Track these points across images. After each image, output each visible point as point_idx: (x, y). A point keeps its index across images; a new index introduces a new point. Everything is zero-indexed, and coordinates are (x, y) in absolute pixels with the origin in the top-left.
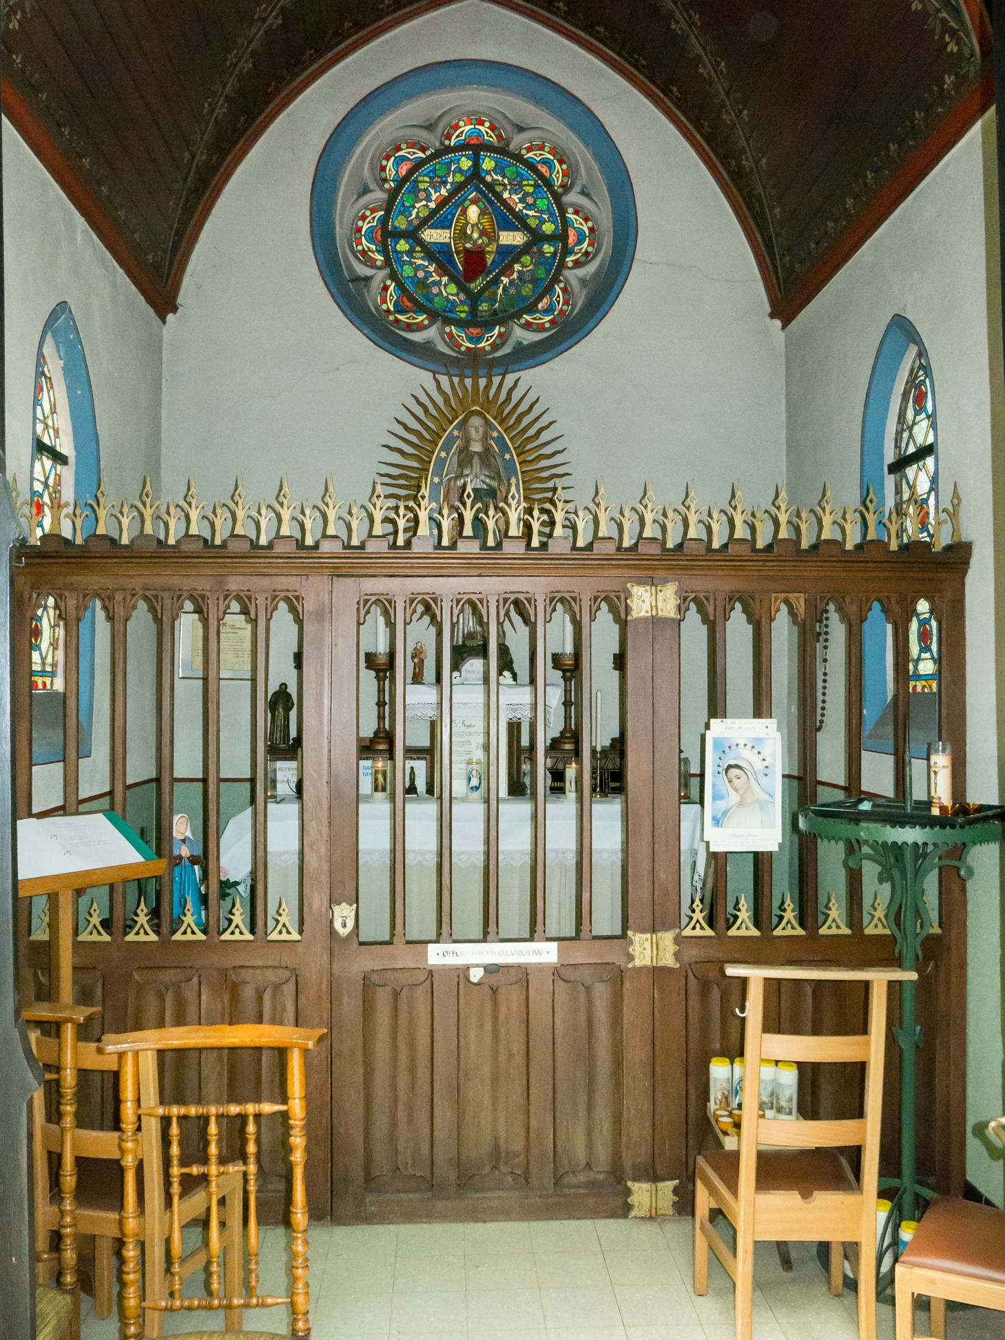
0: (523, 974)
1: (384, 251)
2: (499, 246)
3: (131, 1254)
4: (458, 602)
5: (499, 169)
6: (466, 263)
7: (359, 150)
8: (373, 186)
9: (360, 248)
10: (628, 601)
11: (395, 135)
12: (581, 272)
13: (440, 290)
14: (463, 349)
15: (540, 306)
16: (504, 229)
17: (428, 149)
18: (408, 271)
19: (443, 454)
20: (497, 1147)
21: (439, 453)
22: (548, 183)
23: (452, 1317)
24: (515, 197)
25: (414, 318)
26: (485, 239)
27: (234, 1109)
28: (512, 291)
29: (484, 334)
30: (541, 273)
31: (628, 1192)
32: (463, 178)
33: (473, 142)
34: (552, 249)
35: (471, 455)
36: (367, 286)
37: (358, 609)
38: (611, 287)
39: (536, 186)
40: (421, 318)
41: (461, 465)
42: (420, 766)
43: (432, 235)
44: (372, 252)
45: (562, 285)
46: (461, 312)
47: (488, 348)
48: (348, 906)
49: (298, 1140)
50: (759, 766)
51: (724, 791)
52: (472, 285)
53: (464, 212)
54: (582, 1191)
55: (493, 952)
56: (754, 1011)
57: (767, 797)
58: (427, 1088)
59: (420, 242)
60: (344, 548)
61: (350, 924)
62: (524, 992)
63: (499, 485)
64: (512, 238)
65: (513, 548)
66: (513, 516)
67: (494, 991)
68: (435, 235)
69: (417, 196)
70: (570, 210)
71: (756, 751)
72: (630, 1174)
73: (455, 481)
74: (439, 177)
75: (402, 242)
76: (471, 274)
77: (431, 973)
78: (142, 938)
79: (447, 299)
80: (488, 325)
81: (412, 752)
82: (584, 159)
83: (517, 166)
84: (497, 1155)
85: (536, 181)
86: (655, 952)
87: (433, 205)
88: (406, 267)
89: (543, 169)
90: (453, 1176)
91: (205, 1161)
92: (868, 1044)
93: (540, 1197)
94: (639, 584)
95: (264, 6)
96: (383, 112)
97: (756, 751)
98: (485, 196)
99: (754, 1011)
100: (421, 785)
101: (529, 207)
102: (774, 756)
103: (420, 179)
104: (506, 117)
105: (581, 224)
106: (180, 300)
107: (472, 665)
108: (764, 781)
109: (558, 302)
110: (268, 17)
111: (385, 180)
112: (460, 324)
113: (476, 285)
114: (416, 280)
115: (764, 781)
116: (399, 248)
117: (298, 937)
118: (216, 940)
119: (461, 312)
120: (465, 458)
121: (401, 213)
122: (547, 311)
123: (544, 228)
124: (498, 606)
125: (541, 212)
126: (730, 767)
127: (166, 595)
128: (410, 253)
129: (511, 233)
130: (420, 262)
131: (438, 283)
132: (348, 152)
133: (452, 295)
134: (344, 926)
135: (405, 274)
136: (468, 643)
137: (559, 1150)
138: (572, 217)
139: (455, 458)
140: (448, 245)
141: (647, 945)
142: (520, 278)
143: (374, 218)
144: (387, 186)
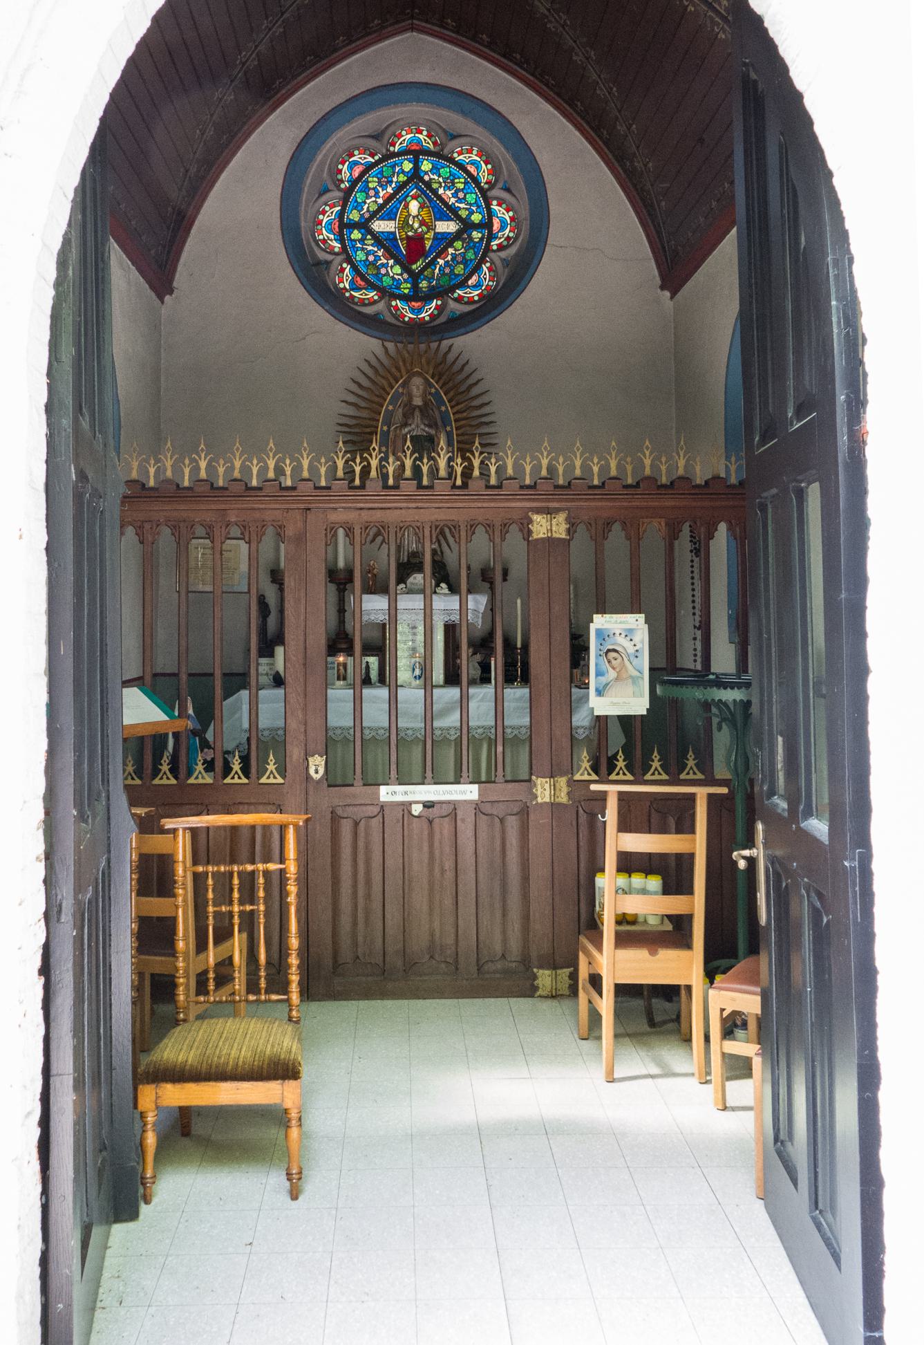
0: (453, 809)
1: (341, 240)
3: (181, 964)
4: (401, 528)
5: (435, 169)
6: (408, 248)
7: (319, 158)
8: (331, 186)
9: (321, 237)
10: (530, 526)
11: (350, 144)
12: (503, 254)
13: (387, 271)
14: (406, 319)
15: (470, 282)
17: (376, 155)
18: (361, 256)
19: (391, 408)
20: (432, 941)
21: (387, 406)
22: (475, 181)
23: (398, 1050)
24: (449, 193)
25: (366, 295)
27: (250, 868)
28: (447, 270)
29: (424, 306)
30: (470, 255)
31: (535, 977)
32: (406, 178)
33: (413, 148)
34: (480, 235)
36: (328, 268)
37: (326, 534)
38: (529, 265)
40: (372, 294)
42: (373, 661)
43: (380, 226)
44: (331, 240)
45: (488, 265)
46: (404, 288)
47: (427, 318)
48: (319, 758)
49: (292, 888)
50: (631, 650)
51: (605, 670)
52: (414, 267)
53: (406, 206)
54: (498, 976)
55: (429, 792)
56: (611, 815)
57: (638, 674)
59: (370, 232)
61: (322, 771)
62: (453, 823)
63: (436, 432)
65: (442, 487)
67: (431, 822)
68: (382, 226)
69: (367, 194)
70: (495, 202)
71: (628, 638)
72: (536, 963)
73: (401, 429)
74: (385, 177)
75: (356, 232)
78: (165, 781)
79: (393, 278)
80: (427, 298)
81: (368, 649)
83: (450, 167)
85: (466, 179)
86: (553, 792)
87: (380, 201)
88: (358, 253)
89: (472, 169)
90: (399, 963)
91: (231, 903)
92: (694, 841)
93: (467, 980)
94: (538, 513)
95: (244, 53)
96: (340, 126)
97: (628, 638)
98: (423, 192)
99: (611, 815)
100: (374, 674)
101: (460, 200)
102: (642, 642)
103: (370, 179)
104: (441, 127)
105: (503, 214)
106: (175, 284)
107: (415, 578)
108: (635, 661)
109: (485, 279)
110: (246, 61)
111: (342, 181)
114: (368, 263)
116: (353, 237)
118: (220, 783)
119: (404, 288)
120: (409, 411)
121: (355, 208)
122: (475, 286)
123: (473, 218)
124: (431, 531)
125: (471, 204)
126: (609, 651)
128: (362, 240)
129: (446, 223)
130: (370, 248)
131: (385, 266)
132: (311, 159)
133: (397, 274)
134: (317, 772)
135: (358, 258)
137: (481, 946)
138: (497, 208)
139: (400, 410)
141: (547, 786)
142: (453, 259)
143: (332, 213)
144: (343, 186)
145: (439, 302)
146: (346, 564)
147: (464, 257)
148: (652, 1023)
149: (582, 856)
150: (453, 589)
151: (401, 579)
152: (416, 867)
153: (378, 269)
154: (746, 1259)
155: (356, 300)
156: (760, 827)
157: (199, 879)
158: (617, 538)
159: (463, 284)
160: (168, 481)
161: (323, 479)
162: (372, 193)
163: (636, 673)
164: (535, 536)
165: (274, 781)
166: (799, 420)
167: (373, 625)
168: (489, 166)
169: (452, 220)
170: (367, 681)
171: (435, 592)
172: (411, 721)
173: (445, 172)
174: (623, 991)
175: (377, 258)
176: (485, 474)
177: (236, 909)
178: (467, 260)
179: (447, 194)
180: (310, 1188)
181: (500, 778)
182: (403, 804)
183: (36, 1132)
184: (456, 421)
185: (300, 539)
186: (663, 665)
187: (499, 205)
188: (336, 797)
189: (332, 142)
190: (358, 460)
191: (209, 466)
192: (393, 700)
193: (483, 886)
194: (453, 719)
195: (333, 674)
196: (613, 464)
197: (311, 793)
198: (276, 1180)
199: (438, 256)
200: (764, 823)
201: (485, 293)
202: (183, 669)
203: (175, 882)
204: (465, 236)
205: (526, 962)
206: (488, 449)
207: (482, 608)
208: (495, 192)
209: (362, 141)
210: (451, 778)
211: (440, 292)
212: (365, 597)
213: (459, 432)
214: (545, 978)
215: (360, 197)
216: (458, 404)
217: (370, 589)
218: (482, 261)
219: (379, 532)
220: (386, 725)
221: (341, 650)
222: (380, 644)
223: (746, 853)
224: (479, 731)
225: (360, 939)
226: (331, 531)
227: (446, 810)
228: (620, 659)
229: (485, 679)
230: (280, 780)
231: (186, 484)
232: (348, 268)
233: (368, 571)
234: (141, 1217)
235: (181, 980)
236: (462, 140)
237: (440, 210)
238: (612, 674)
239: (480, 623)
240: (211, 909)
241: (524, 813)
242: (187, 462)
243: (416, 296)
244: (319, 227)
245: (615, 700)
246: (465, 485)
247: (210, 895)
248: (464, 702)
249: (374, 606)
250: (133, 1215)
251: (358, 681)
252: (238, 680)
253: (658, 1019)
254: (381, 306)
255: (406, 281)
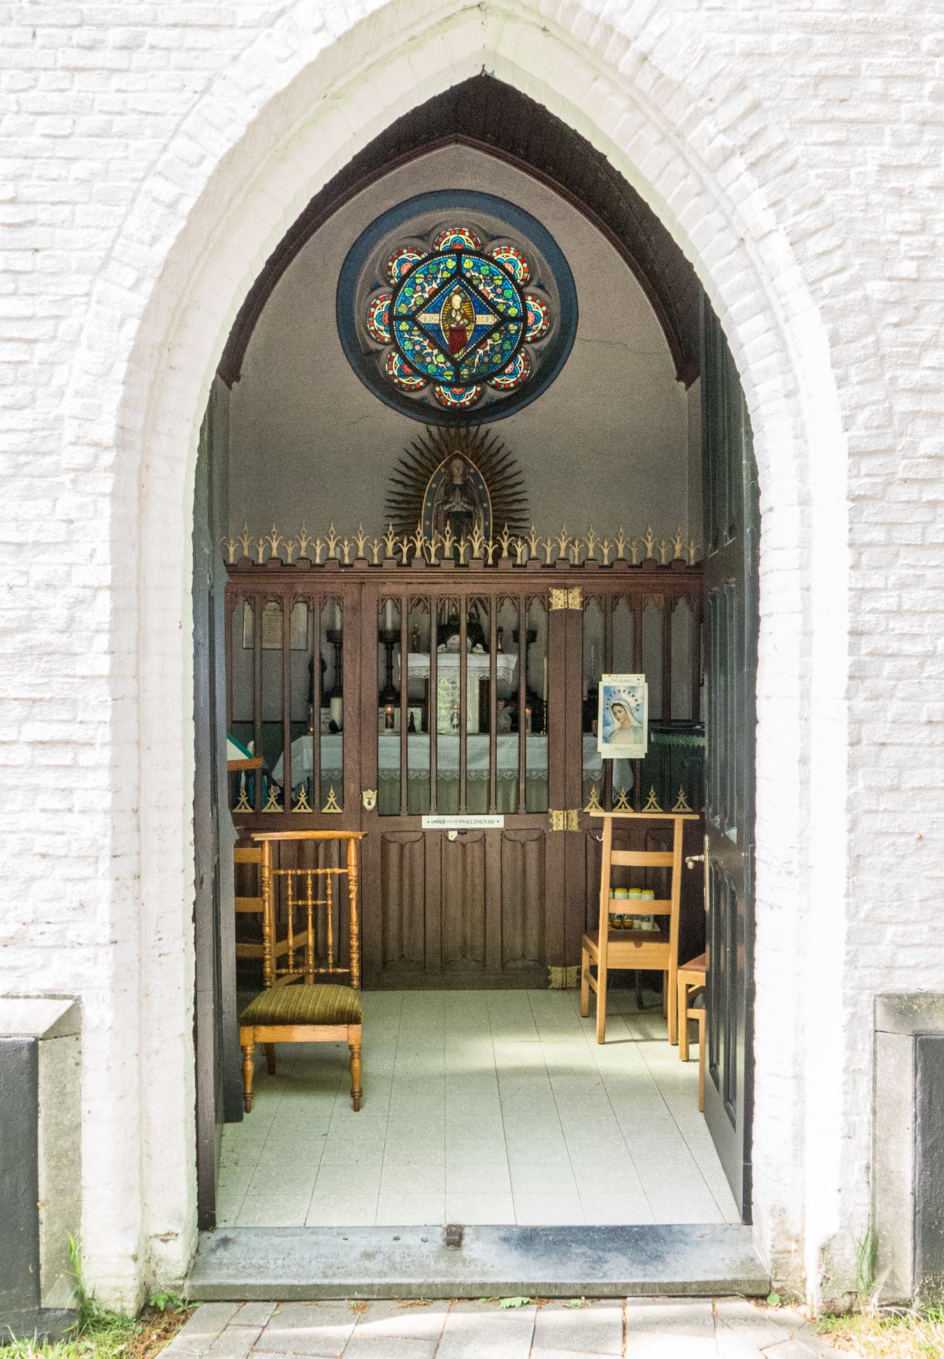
0: (482, 836)
1: (391, 332)
2: (476, 326)
5: (476, 267)
7: (372, 256)
8: (382, 282)
9: (372, 328)
12: (536, 346)
14: (449, 404)
16: (480, 313)
24: (488, 289)
26: (466, 321)
28: (486, 360)
30: (507, 346)
31: (549, 973)
34: (516, 327)
35: (455, 487)
36: (378, 358)
39: (503, 280)
41: (447, 493)
42: (417, 712)
43: (426, 318)
47: (468, 403)
49: (353, 888)
50: (633, 704)
52: (456, 356)
53: (450, 301)
56: (606, 837)
58: (422, 907)
59: (417, 324)
60: (370, 566)
61: (373, 803)
64: (487, 320)
65: (476, 566)
66: (476, 545)
67: (464, 846)
70: (530, 298)
75: (404, 323)
76: (455, 349)
77: (424, 833)
78: (243, 810)
80: (468, 385)
81: (413, 702)
82: (540, 262)
84: (465, 949)
87: (426, 296)
89: (509, 267)
98: (466, 288)
99: (606, 837)
100: (418, 723)
101: (498, 296)
102: (643, 698)
106: (242, 372)
108: (636, 714)
111: (392, 277)
112: (449, 385)
113: (459, 356)
115: (636, 714)
116: (401, 328)
117: (340, 811)
120: (450, 489)
121: (403, 302)
122: (512, 374)
123: (510, 312)
125: (508, 299)
126: (614, 705)
127: (257, 596)
128: (409, 331)
130: (417, 338)
131: (430, 355)
134: (369, 804)
136: (452, 623)
138: (531, 303)
139: (443, 489)
140: (438, 325)
144: (392, 281)
145: (479, 389)
146: (394, 627)
147: (501, 348)
148: (641, 1005)
149: (589, 878)
150: (487, 649)
151: (442, 640)
152: (451, 882)
153: (424, 357)
154: (684, 1144)
155: (404, 386)
156: (707, 838)
157: (279, 881)
158: (622, 607)
159: (500, 372)
160: (244, 558)
161: (376, 558)
162: (418, 288)
163: (636, 724)
164: (554, 608)
165: (334, 811)
166: (731, 538)
167: (418, 680)
168: (525, 265)
169: (491, 313)
170: (411, 729)
171: (472, 652)
172: (448, 765)
173: (485, 270)
174: (611, 973)
175: (423, 348)
176: (512, 554)
177: (310, 903)
178: (504, 351)
179: (487, 290)
180: (370, 1104)
181: (522, 810)
182: (441, 831)
183: (192, 1024)
184: (492, 498)
185: (357, 608)
186: (659, 717)
187: (534, 300)
188: (385, 825)
189: (382, 243)
190: (405, 542)
191: (279, 546)
192: (433, 746)
193: (507, 894)
194: (484, 764)
195: (382, 722)
196: (621, 547)
197: (365, 821)
198: (341, 1102)
199: (479, 345)
200: (709, 835)
201: (520, 380)
202: (258, 718)
203: (263, 882)
204: (503, 328)
205: (542, 961)
206: (516, 532)
207: (513, 666)
208: (530, 289)
209: (410, 241)
210: (485, 810)
211: (481, 379)
212: (410, 655)
213: (496, 508)
214: (557, 974)
215: (408, 291)
216: (494, 483)
217: (415, 650)
218: (518, 351)
219: (419, 601)
220: (428, 767)
221: (390, 702)
222: (424, 699)
223: (696, 858)
224: (508, 773)
225: (405, 943)
226: (382, 601)
227: (479, 835)
228: (623, 712)
229: (515, 728)
230: (339, 810)
231: (261, 561)
232: (396, 357)
233: (414, 632)
234: (244, 1120)
235: (268, 957)
236: (502, 241)
237: (481, 305)
238: (617, 724)
239: (511, 678)
240: (290, 903)
241: (542, 839)
242: (261, 542)
243: (458, 383)
244: (371, 319)
245: (619, 746)
246: (495, 565)
247: (290, 892)
248: (492, 749)
249: (418, 663)
250: (239, 1118)
251: (404, 729)
252: (301, 728)
253: (646, 1004)
254: (425, 392)
255: (449, 369)
